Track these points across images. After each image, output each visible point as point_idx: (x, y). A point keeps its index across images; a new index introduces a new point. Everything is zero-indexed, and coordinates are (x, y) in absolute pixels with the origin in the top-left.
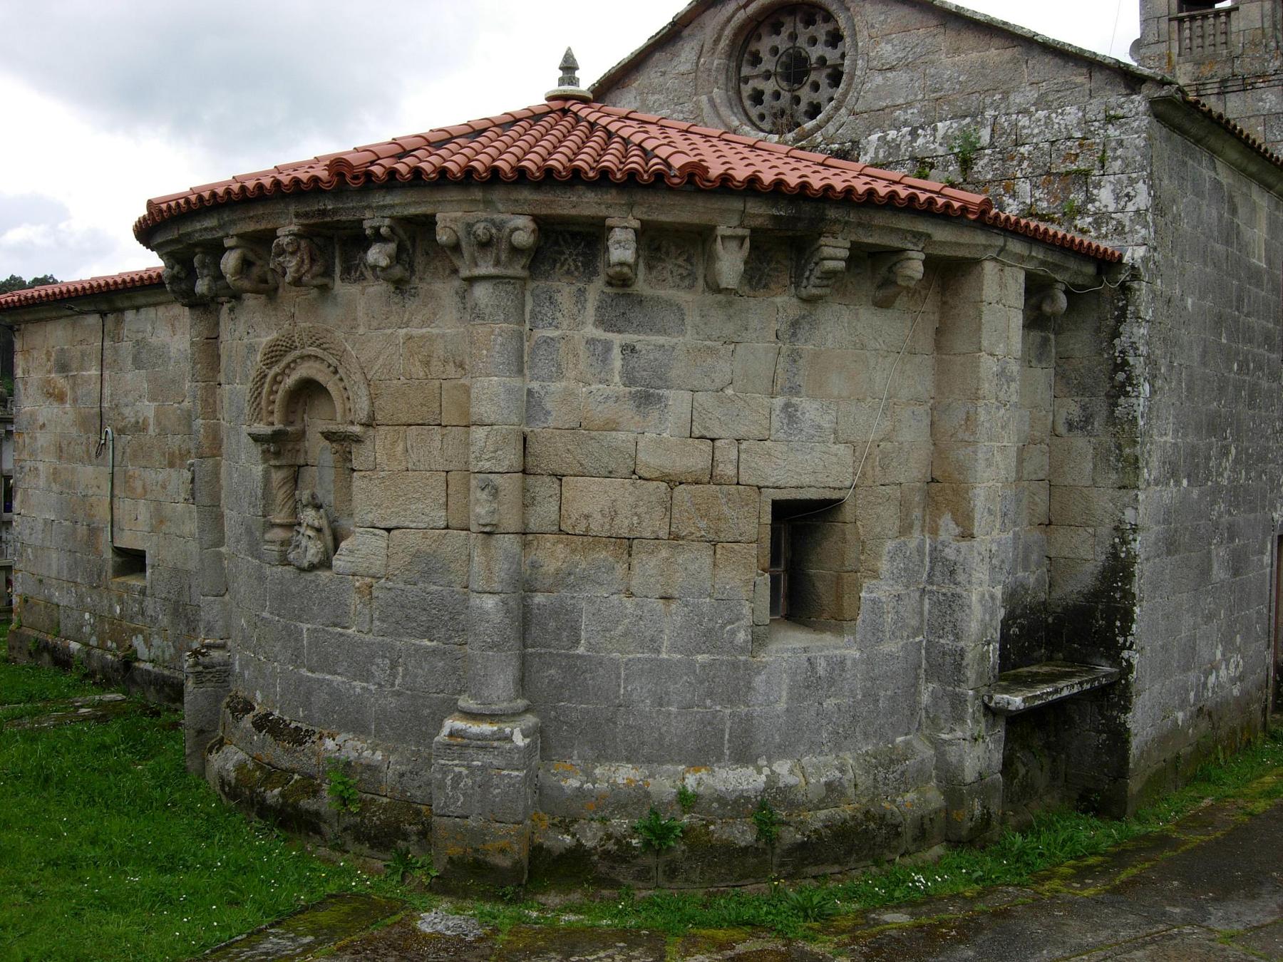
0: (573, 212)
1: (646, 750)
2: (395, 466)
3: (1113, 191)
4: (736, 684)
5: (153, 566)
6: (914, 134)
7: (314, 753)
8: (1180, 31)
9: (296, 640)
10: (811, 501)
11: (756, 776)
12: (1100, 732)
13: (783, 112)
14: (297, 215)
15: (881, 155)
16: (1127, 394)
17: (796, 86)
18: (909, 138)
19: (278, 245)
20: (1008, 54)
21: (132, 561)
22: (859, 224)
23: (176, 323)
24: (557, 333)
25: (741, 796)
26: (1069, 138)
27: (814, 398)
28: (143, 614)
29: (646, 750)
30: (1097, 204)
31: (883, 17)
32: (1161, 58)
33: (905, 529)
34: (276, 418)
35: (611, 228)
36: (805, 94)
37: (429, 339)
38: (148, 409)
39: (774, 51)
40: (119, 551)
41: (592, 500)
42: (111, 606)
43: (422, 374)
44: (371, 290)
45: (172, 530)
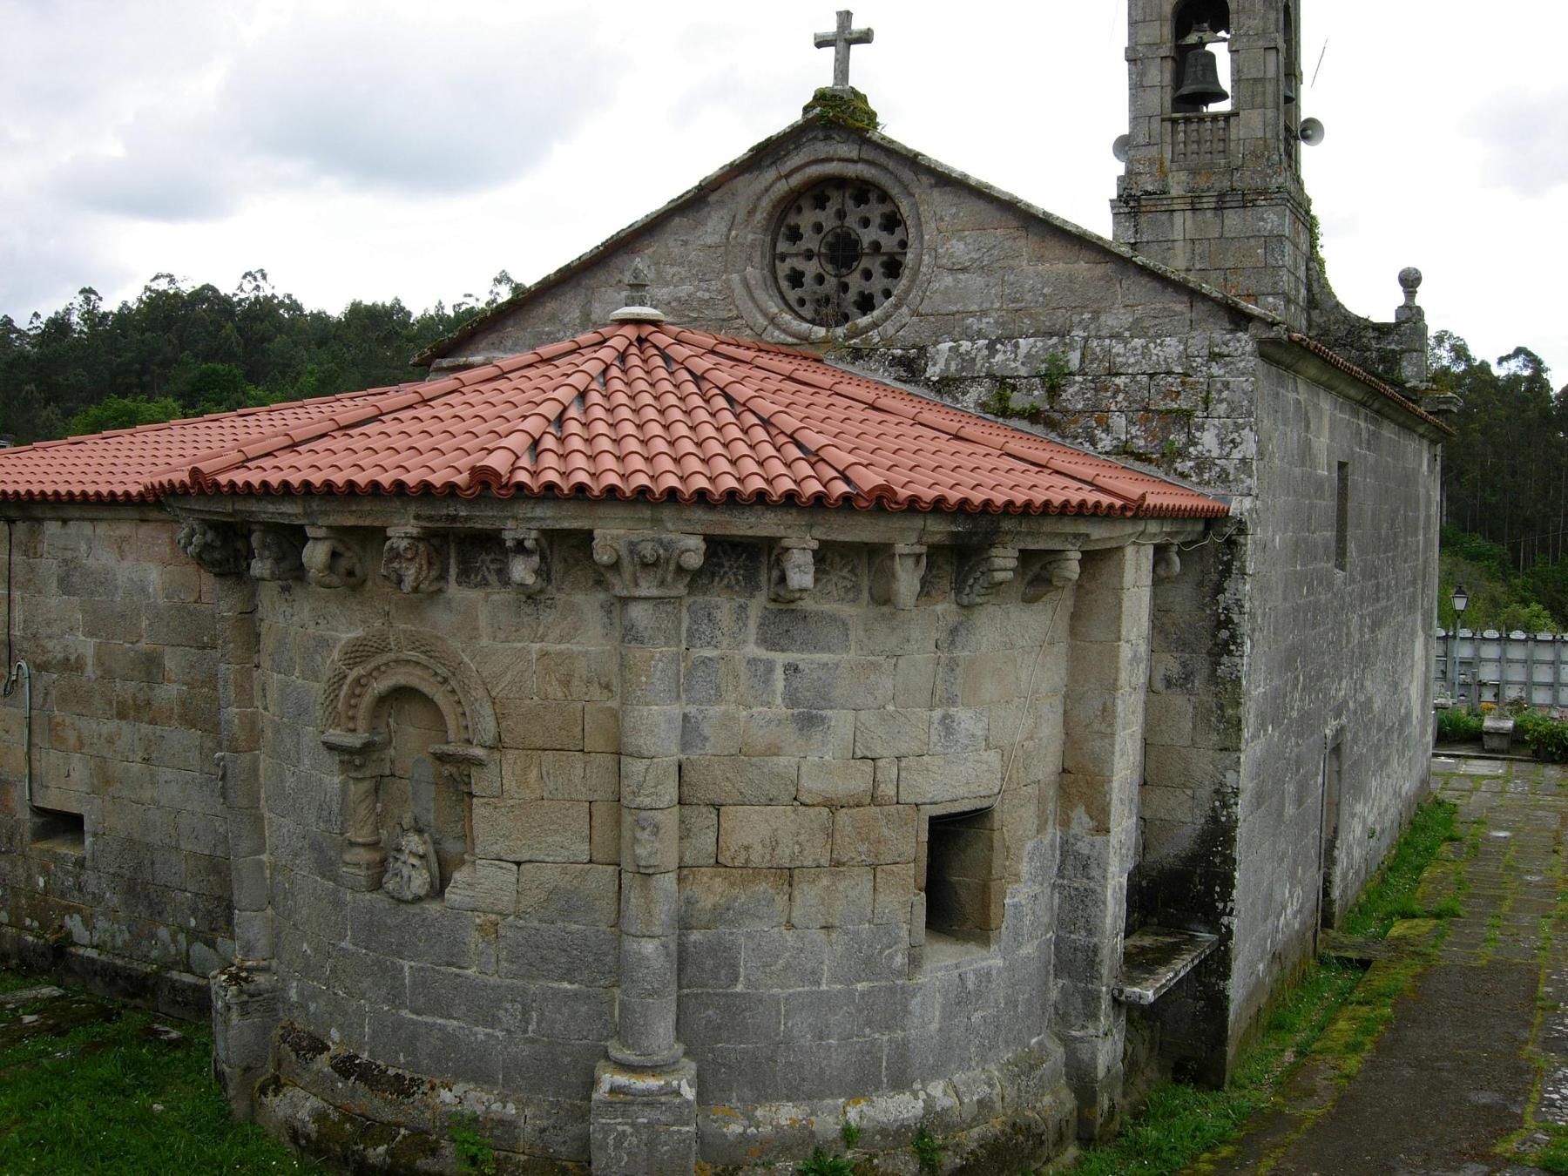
0: (750, 533)
1: (806, 1087)
3: (1217, 435)
4: (891, 1008)
5: (95, 835)
6: (991, 347)
7: (427, 1106)
8: (1174, 132)
9: (394, 978)
10: (964, 813)
11: (913, 1103)
12: (1197, 999)
13: (828, 300)
14: (417, 517)
15: (953, 367)
16: (1230, 653)
17: (844, 271)
18: (986, 352)
19: (391, 548)
20: (1100, 270)
21: (67, 824)
22: (1029, 533)
23: (126, 547)
24: (715, 653)
25: (902, 1125)
26: (1169, 373)
27: (968, 706)
28: (80, 890)
29: (806, 1087)
30: (1200, 448)
31: (954, 210)
32: (1151, 162)
33: (1041, 829)
34: (361, 724)
35: (787, 549)
36: (855, 281)
37: (570, 656)
38: (85, 646)
39: (818, 228)
40: (39, 811)
41: (752, 830)
42: (29, 877)
43: (560, 695)
44: (495, 597)
45: (124, 793)
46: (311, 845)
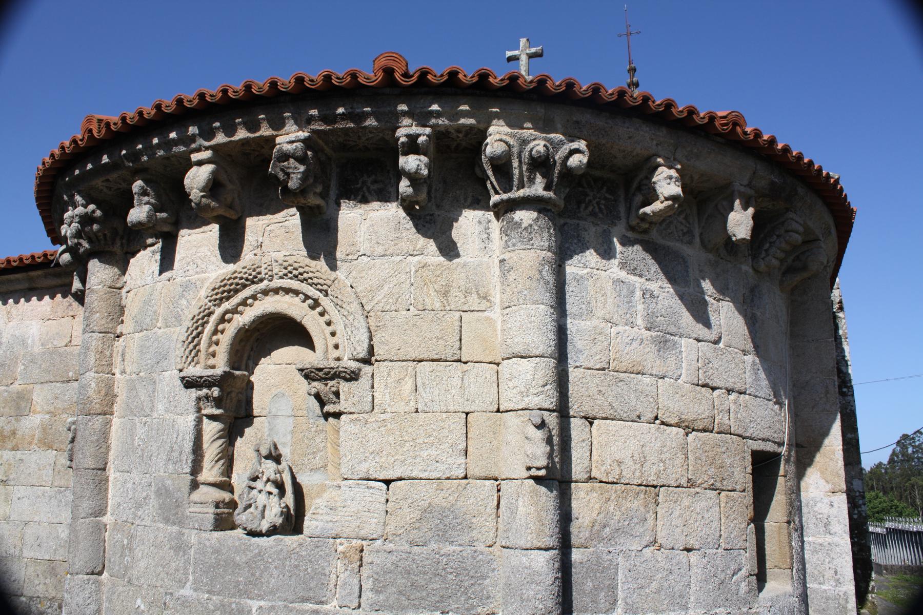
2: (401, 407)
43: (438, 305)
46: (158, 493)
